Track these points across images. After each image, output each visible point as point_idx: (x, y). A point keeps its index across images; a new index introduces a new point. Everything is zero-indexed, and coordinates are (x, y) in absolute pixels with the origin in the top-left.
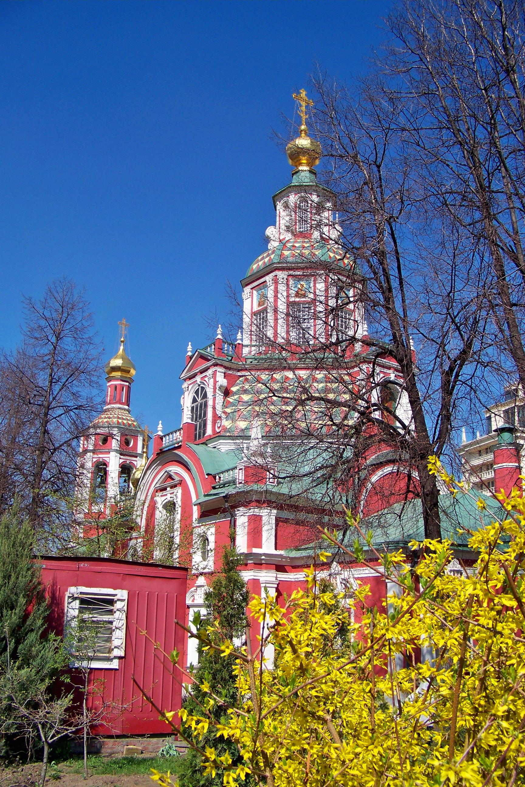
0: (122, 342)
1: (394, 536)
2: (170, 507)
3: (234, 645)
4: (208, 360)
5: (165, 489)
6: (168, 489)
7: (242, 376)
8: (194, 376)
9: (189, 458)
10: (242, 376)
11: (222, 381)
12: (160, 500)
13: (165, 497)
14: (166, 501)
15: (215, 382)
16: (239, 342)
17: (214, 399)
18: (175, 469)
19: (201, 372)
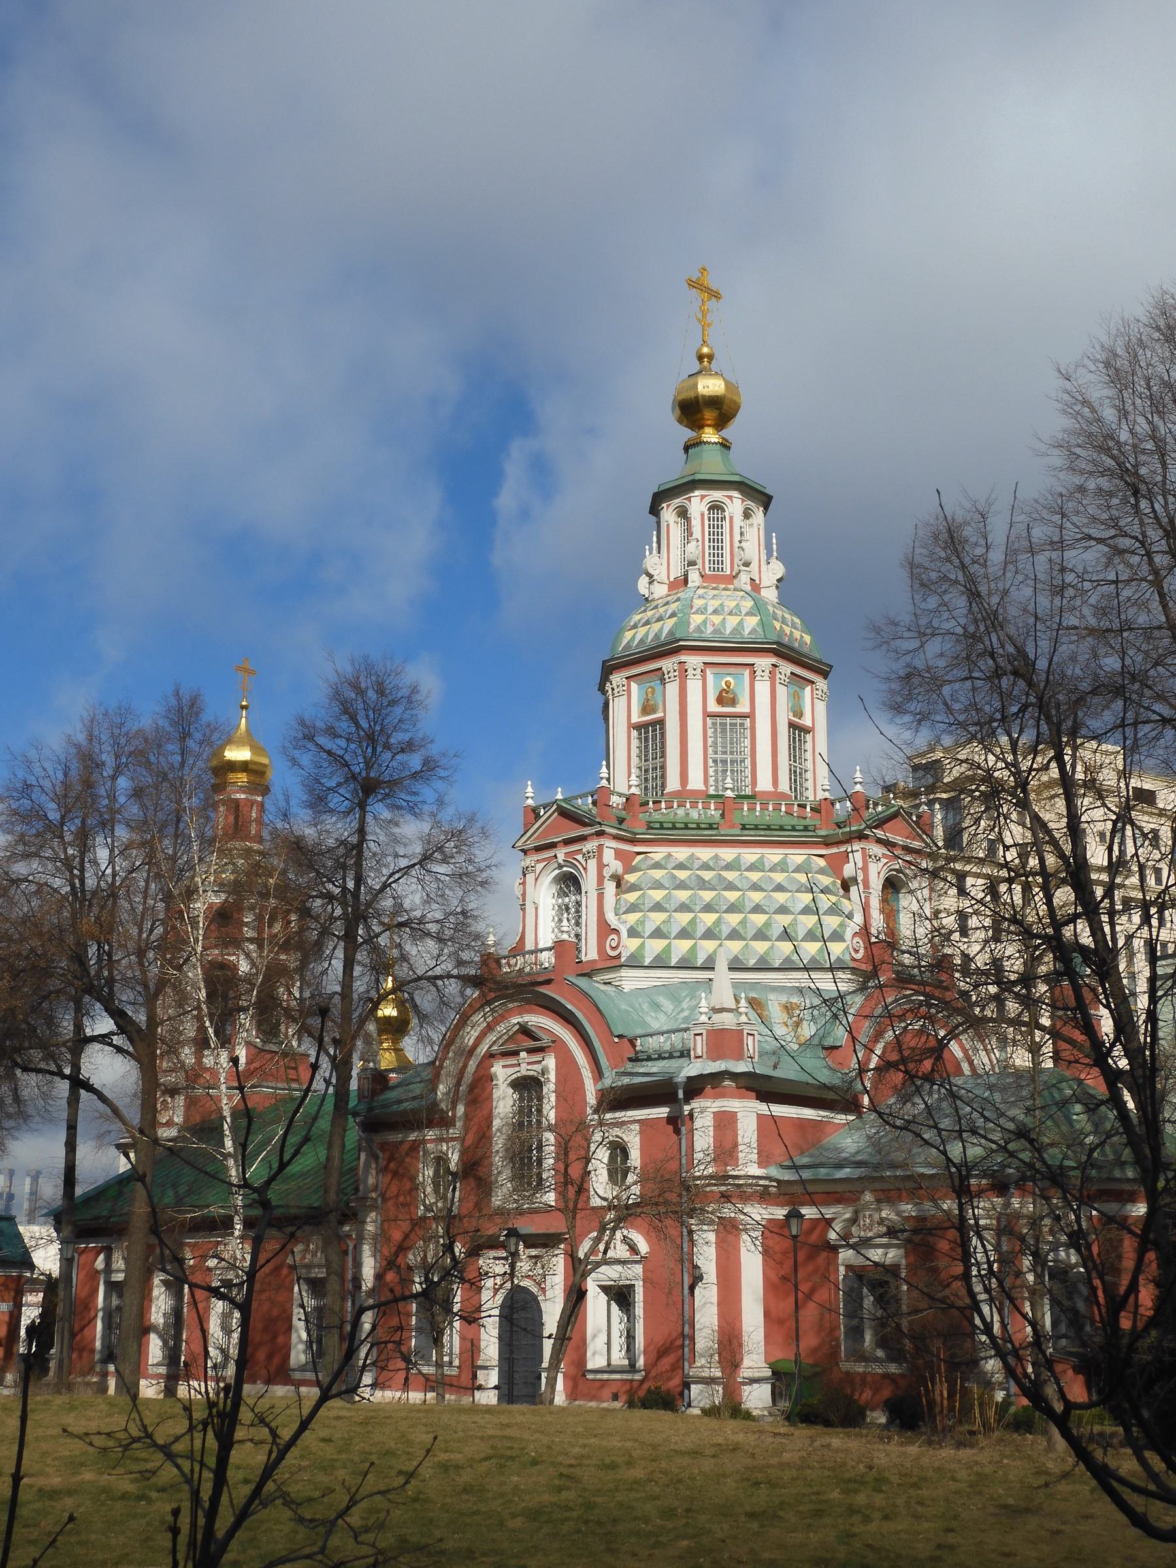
0: (243, 707)
1: (414, 953)
2: (528, 1086)
3: (113, 1034)
4: (585, 825)
5: (515, 1053)
6: (523, 1054)
7: (639, 853)
8: (553, 846)
9: (584, 1015)
10: (639, 853)
11: (614, 866)
12: (502, 1072)
13: (517, 1069)
14: (519, 1075)
15: (601, 866)
16: (604, 783)
17: (601, 897)
18: (539, 1020)
19: (567, 842)
